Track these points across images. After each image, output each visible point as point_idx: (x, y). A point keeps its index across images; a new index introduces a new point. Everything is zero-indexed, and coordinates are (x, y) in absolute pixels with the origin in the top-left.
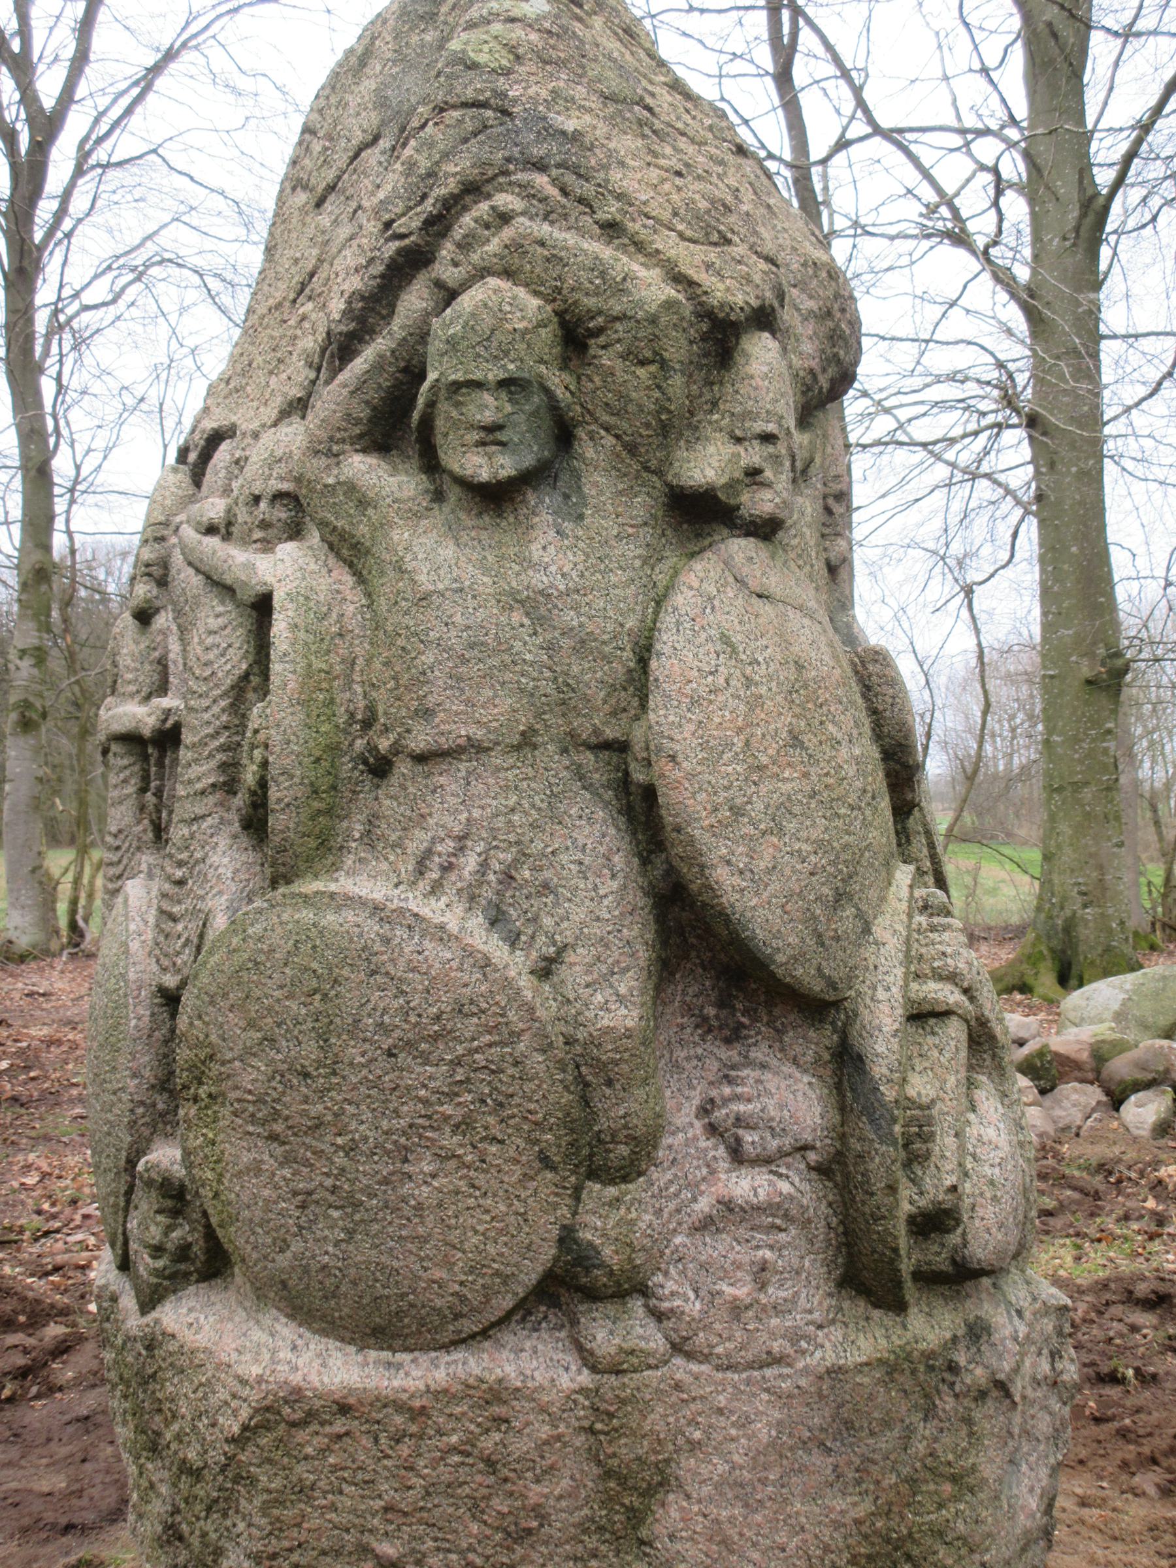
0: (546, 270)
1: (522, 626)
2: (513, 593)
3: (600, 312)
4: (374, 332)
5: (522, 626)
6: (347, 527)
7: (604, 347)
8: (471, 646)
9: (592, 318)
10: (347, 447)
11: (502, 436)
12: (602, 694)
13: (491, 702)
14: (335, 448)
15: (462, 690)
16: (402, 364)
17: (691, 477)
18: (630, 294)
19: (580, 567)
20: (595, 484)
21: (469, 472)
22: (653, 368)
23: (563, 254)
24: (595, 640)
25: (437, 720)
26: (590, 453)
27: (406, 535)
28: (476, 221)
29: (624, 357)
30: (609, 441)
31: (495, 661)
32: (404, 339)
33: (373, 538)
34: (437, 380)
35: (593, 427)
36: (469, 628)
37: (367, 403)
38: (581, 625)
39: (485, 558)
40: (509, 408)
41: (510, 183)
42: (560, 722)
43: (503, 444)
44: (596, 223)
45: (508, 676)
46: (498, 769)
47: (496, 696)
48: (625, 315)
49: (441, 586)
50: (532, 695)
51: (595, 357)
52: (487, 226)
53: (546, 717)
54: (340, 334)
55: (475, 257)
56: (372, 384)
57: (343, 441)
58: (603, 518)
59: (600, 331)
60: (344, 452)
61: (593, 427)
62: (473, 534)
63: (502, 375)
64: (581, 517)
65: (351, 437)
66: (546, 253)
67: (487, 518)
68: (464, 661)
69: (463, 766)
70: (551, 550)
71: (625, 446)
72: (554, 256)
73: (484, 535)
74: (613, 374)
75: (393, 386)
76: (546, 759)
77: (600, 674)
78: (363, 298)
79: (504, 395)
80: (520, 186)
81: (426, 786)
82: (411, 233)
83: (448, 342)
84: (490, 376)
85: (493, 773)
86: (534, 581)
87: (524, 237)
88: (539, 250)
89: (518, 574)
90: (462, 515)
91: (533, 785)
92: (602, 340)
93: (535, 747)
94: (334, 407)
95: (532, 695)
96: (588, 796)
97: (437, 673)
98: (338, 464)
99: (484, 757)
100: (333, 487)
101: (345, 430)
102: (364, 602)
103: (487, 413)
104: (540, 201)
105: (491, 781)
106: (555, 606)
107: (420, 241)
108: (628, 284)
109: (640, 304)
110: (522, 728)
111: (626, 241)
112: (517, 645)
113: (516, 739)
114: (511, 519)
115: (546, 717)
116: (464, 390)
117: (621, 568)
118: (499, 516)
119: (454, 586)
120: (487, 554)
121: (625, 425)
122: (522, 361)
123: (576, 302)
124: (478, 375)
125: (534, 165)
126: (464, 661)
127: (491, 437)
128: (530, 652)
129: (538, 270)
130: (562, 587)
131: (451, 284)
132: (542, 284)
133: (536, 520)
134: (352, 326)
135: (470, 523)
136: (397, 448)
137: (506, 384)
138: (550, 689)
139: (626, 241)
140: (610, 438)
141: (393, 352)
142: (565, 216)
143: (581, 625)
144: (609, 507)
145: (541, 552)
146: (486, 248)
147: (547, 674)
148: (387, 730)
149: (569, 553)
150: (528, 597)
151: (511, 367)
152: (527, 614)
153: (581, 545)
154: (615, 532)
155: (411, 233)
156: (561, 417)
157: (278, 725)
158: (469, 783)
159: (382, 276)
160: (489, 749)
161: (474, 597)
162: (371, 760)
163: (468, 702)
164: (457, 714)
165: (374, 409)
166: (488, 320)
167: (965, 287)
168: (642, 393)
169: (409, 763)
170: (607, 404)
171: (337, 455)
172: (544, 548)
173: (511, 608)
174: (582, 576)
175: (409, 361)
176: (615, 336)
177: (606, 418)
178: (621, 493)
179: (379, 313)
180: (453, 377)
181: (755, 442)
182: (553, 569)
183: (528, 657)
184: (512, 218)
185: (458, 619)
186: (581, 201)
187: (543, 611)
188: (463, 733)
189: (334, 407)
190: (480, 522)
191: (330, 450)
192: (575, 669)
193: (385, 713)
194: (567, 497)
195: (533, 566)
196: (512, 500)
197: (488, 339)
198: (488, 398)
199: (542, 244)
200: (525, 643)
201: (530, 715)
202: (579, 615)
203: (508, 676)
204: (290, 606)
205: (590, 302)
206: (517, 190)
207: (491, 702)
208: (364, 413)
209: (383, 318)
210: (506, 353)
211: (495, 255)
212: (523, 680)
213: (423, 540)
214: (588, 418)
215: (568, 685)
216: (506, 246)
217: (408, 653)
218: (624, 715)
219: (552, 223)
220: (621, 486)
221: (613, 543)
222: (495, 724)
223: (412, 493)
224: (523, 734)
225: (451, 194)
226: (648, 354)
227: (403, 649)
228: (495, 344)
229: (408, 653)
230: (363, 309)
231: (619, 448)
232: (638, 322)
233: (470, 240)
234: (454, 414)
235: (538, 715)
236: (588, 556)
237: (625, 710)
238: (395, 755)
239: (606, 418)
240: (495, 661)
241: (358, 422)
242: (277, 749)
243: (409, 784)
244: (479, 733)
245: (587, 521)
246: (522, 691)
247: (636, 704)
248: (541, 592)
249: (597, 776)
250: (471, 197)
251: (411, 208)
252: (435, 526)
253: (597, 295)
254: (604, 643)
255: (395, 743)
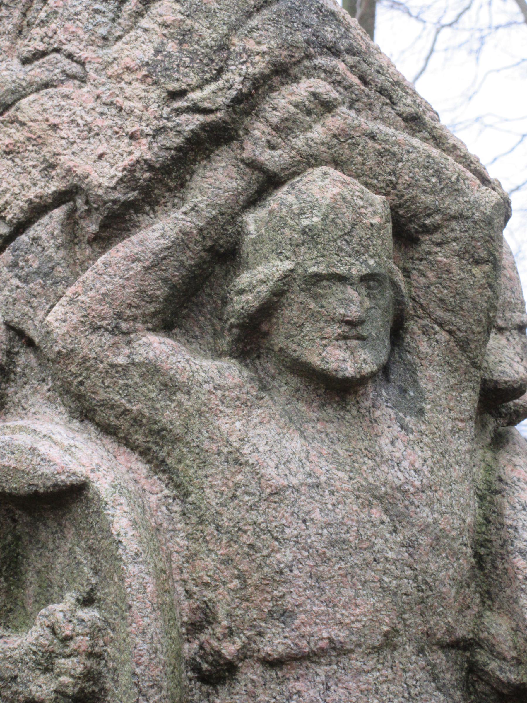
0: (379, 164)
1: (382, 523)
2: (371, 489)
3: (437, 211)
4: (158, 203)
5: (382, 523)
6: (147, 412)
7: (439, 244)
8: (332, 544)
9: (429, 215)
10: (139, 325)
11: (363, 331)
12: (454, 591)
13: (352, 603)
14: (124, 326)
15: (323, 590)
16: (209, 243)
17: (503, 372)
18: (464, 194)
19: (429, 462)
20: (431, 379)
21: (332, 366)
22: (486, 268)
23: (395, 149)
24: (447, 537)
25: (297, 622)
26: (424, 347)
27: (238, 425)
28: (296, 106)
29: (459, 255)
30: (443, 336)
31: (357, 560)
32: (214, 218)
33: (186, 426)
34: (292, 271)
35: (426, 322)
36: (329, 525)
37: (165, 280)
38: (436, 522)
39: (335, 452)
40: (367, 303)
41: (315, 68)
42: (419, 621)
43: (361, 338)
44: (400, 115)
45: (370, 575)
46: (360, 672)
47: (357, 595)
48: (462, 215)
49: (294, 481)
50: (395, 594)
51: (429, 253)
52: (309, 113)
53: (406, 616)
54: (114, 202)
55: (299, 142)
56: (172, 262)
57: (135, 319)
58: (440, 412)
59: (436, 228)
60: (135, 331)
61: (426, 322)
62: (319, 426)
63: (365, 271)
64: (421, 412)
65: (144, 315)
66: (378, 147)
67: (330, 411)
68: (325, 559)
69: (321, 670)
70: (399, 444)
71: (458, 342)
72: (386, 150)
73: (331, 428)
74: (449, 272)
75: (196, 265)
76: (404, 660)
77: (451, 571)
78: (151, 168)
79: (363, 291)
80: (325, 71)
81: (281, 693)
82: (218, 109)
83: (304, 233)
84: (354, 271)
85: (354, 677)
86: (390, 477)
87: (354, 128)
88: (370, 143)
89: (373, 470)
90: (301, 406)
91: (392, 688)
92: (437, 237)
93: (395, 647)
94: (121, 281)
95: (395, 594)
96: (442, 698)
97: (296, 572)
98: (129, 343)
99: (344, 660)
100: (125, 368)
101: (138, 307)
102: (166, 492)
103: (353, 308)
104: (345, 88)
105: (352, 685)
106: (412, 503)
107: (227, 119)
108: (461, 184)
109: (475, 205)
110: (385, 628)
111: (426, 135)
112: (379, 543)
113: (377, 640)
114: (354, 412)
115: (406, 616)
116: (325, 283)
117: (457, 463)
118: (343, 408)
119: (309, 481)
120: (337, 447)
121: (459, 322)
122: (379, 256)
123: (413, 199)
124: (341, 270)
125: (329, 49)
126: (325, 559)
127: (354, 332)
128: (391, 549)
129: (370, 163)
130: (417, 483)
131: (271, 166)
132: (375, 177)
133: (378, 413)
134: (133, 195)
135: (313, 416)
136: (180, 326)
137: (366, 279)
138: (410, 587)
139: (426, 135)
140: (444, 333)
141: (201, 230)
142: (370, 106)
143: (436, 522)
144: (444, 401)
145: (390, 446)
146: (309, 135)
147: (409, 572)
148: (231, 633)
149: (417, 449)
150: (386, 493)
151: (371, 262)
152: (386, 511)
153: (426, 440)
154: (449, 427)
155: (218, 109)
156: (402, 310)
157: (144, 633)
158: (328, 688)
159: (178, 149)
160: (351, 651)
161: (332, 493)
162: (205, 666)
163: (328, 603)
164: (318, 615)
165: (173, 287)
166: (349, 215)
167: (513, 149)
168: (477, 292)
169: (259, 669)
170: (442, 300)
171: (127, 334)
172: (392, 443)
173: (370, 505)
174: (432, 472)
175: (216, 241)
176: (453, 235)
177: (439, 313)
178: (452, 388)
179: (166, 185)
180: (314, 269)
181: (513, 332)
182: (405, 464)
183: (390, 555)
184: (335, 107)
185: (316, 515)
186: (382, 91)
187: (401, 507)
188: (325, 635)
189: (121, 281)
190: (323, 414)
191: (117, 327)
192: (432, 567)
193: (229, 615)
194: (403, 391)
195: (385, 461)
196: (356, 392)
197: (349, 233)
198: (351, 292)
199: (373, 137)
200: (386, 541)
201: (393, 615)
202: (433, 511)
203: (370, 575)
204: (123, 500)
205: (428, 199)
206: (323, 75)
207: (352, 603)
208: (162, 291)
209: (170, 190)
210: (367, 249)
211: (323, 144)
212: (386, 579)
213: (260, 430)
214: (420, 312)
215: (427, 583)
216: (335, 136)
217: (259, 550)
218: (468, 612)
219: (358, 111)
220: (452, 381)
221: (449, 437)
222: (358, 625)
223: (237, 380)
224: (386, 635)
225: (262, 74)
226: (484, 254)
227: (251, 546)
228: (356, 239)
229: (259, 550)
230: (150, 180)
231: (452, 344)
232: (475, 222)
233: (289, 124)
234: (313, 305)
235: (400, 616)
236: (433, 451)
237: (469, 607)
238: (242, 660)
239: (439, 313)
240: (357, 560)
241: (153, 299)
242: (145, 659)
243: (260, 691)
244: (342, 635)
245: (428, 415)
246: (385, 590)
247: (478, 601)
248: (398, 489)
249: (448, 676)
250: (279, 78)
251: (207, 82)
252: (272, 417)
253: (434, 193)
254: (453, 539)
255: (244, 647)
